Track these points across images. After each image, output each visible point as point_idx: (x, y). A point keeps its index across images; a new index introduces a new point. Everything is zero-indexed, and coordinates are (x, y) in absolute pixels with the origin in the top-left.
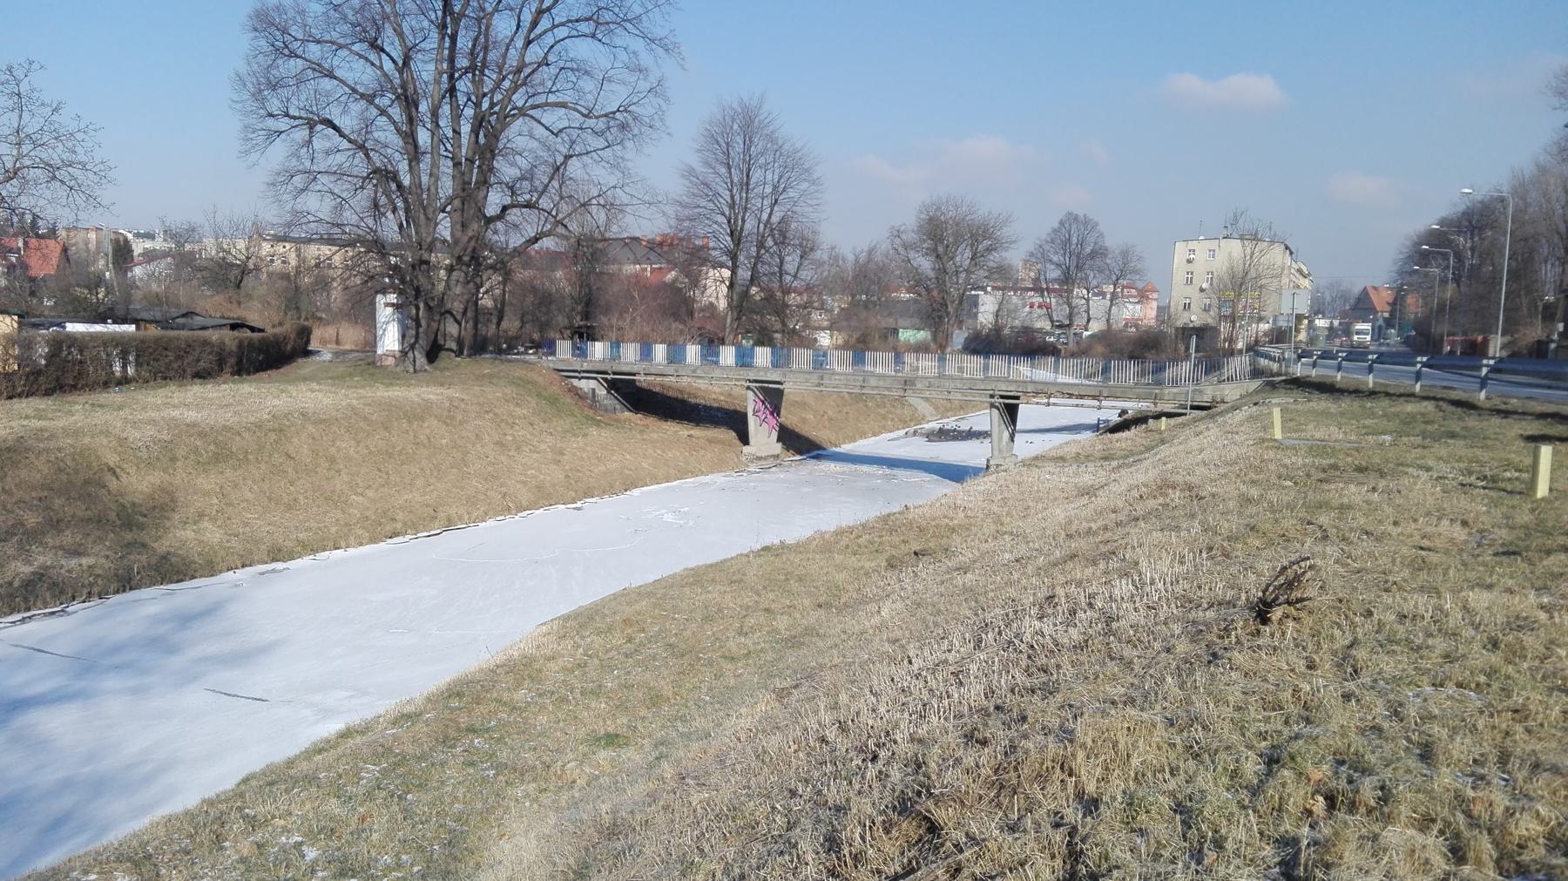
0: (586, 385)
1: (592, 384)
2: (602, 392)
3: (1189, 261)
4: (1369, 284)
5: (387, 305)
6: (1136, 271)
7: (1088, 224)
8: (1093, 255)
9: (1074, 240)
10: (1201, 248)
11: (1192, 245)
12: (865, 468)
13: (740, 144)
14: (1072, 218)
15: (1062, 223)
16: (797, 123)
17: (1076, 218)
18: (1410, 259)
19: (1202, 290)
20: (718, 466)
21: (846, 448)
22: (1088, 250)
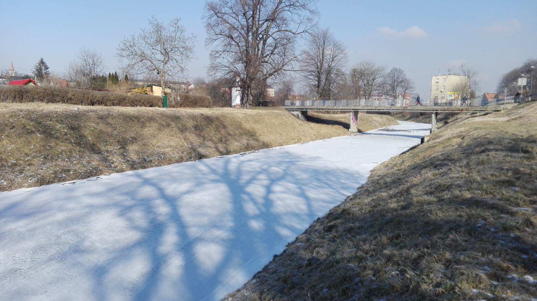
0: (295, 113)
1: (298, 112)
2: (300, 115)
3: (437, 82)
4: (486, 92)
5: (237, 90)
6: (411, 88)
7: (400, 71)
8: (402, 82)
9: (396, 76)
10: (441, 79)
11: (438, 77)
12: (400, 137)
13: (321, 41)
14: (395, 69)
15: (391, 71)
16: (338, 34)
17: (396, 70)
18: (275, 106)
19: (441, 92)
20: (345, 134)
21: (368, 132)
22: (400, 80)
